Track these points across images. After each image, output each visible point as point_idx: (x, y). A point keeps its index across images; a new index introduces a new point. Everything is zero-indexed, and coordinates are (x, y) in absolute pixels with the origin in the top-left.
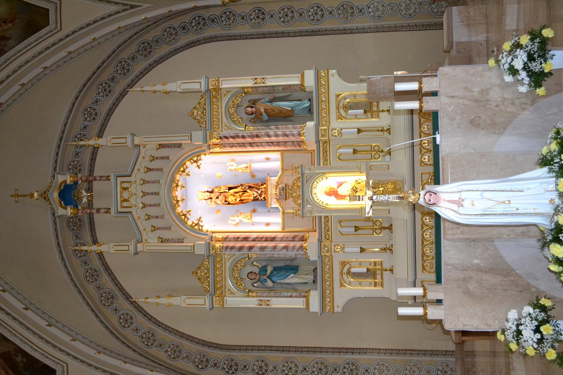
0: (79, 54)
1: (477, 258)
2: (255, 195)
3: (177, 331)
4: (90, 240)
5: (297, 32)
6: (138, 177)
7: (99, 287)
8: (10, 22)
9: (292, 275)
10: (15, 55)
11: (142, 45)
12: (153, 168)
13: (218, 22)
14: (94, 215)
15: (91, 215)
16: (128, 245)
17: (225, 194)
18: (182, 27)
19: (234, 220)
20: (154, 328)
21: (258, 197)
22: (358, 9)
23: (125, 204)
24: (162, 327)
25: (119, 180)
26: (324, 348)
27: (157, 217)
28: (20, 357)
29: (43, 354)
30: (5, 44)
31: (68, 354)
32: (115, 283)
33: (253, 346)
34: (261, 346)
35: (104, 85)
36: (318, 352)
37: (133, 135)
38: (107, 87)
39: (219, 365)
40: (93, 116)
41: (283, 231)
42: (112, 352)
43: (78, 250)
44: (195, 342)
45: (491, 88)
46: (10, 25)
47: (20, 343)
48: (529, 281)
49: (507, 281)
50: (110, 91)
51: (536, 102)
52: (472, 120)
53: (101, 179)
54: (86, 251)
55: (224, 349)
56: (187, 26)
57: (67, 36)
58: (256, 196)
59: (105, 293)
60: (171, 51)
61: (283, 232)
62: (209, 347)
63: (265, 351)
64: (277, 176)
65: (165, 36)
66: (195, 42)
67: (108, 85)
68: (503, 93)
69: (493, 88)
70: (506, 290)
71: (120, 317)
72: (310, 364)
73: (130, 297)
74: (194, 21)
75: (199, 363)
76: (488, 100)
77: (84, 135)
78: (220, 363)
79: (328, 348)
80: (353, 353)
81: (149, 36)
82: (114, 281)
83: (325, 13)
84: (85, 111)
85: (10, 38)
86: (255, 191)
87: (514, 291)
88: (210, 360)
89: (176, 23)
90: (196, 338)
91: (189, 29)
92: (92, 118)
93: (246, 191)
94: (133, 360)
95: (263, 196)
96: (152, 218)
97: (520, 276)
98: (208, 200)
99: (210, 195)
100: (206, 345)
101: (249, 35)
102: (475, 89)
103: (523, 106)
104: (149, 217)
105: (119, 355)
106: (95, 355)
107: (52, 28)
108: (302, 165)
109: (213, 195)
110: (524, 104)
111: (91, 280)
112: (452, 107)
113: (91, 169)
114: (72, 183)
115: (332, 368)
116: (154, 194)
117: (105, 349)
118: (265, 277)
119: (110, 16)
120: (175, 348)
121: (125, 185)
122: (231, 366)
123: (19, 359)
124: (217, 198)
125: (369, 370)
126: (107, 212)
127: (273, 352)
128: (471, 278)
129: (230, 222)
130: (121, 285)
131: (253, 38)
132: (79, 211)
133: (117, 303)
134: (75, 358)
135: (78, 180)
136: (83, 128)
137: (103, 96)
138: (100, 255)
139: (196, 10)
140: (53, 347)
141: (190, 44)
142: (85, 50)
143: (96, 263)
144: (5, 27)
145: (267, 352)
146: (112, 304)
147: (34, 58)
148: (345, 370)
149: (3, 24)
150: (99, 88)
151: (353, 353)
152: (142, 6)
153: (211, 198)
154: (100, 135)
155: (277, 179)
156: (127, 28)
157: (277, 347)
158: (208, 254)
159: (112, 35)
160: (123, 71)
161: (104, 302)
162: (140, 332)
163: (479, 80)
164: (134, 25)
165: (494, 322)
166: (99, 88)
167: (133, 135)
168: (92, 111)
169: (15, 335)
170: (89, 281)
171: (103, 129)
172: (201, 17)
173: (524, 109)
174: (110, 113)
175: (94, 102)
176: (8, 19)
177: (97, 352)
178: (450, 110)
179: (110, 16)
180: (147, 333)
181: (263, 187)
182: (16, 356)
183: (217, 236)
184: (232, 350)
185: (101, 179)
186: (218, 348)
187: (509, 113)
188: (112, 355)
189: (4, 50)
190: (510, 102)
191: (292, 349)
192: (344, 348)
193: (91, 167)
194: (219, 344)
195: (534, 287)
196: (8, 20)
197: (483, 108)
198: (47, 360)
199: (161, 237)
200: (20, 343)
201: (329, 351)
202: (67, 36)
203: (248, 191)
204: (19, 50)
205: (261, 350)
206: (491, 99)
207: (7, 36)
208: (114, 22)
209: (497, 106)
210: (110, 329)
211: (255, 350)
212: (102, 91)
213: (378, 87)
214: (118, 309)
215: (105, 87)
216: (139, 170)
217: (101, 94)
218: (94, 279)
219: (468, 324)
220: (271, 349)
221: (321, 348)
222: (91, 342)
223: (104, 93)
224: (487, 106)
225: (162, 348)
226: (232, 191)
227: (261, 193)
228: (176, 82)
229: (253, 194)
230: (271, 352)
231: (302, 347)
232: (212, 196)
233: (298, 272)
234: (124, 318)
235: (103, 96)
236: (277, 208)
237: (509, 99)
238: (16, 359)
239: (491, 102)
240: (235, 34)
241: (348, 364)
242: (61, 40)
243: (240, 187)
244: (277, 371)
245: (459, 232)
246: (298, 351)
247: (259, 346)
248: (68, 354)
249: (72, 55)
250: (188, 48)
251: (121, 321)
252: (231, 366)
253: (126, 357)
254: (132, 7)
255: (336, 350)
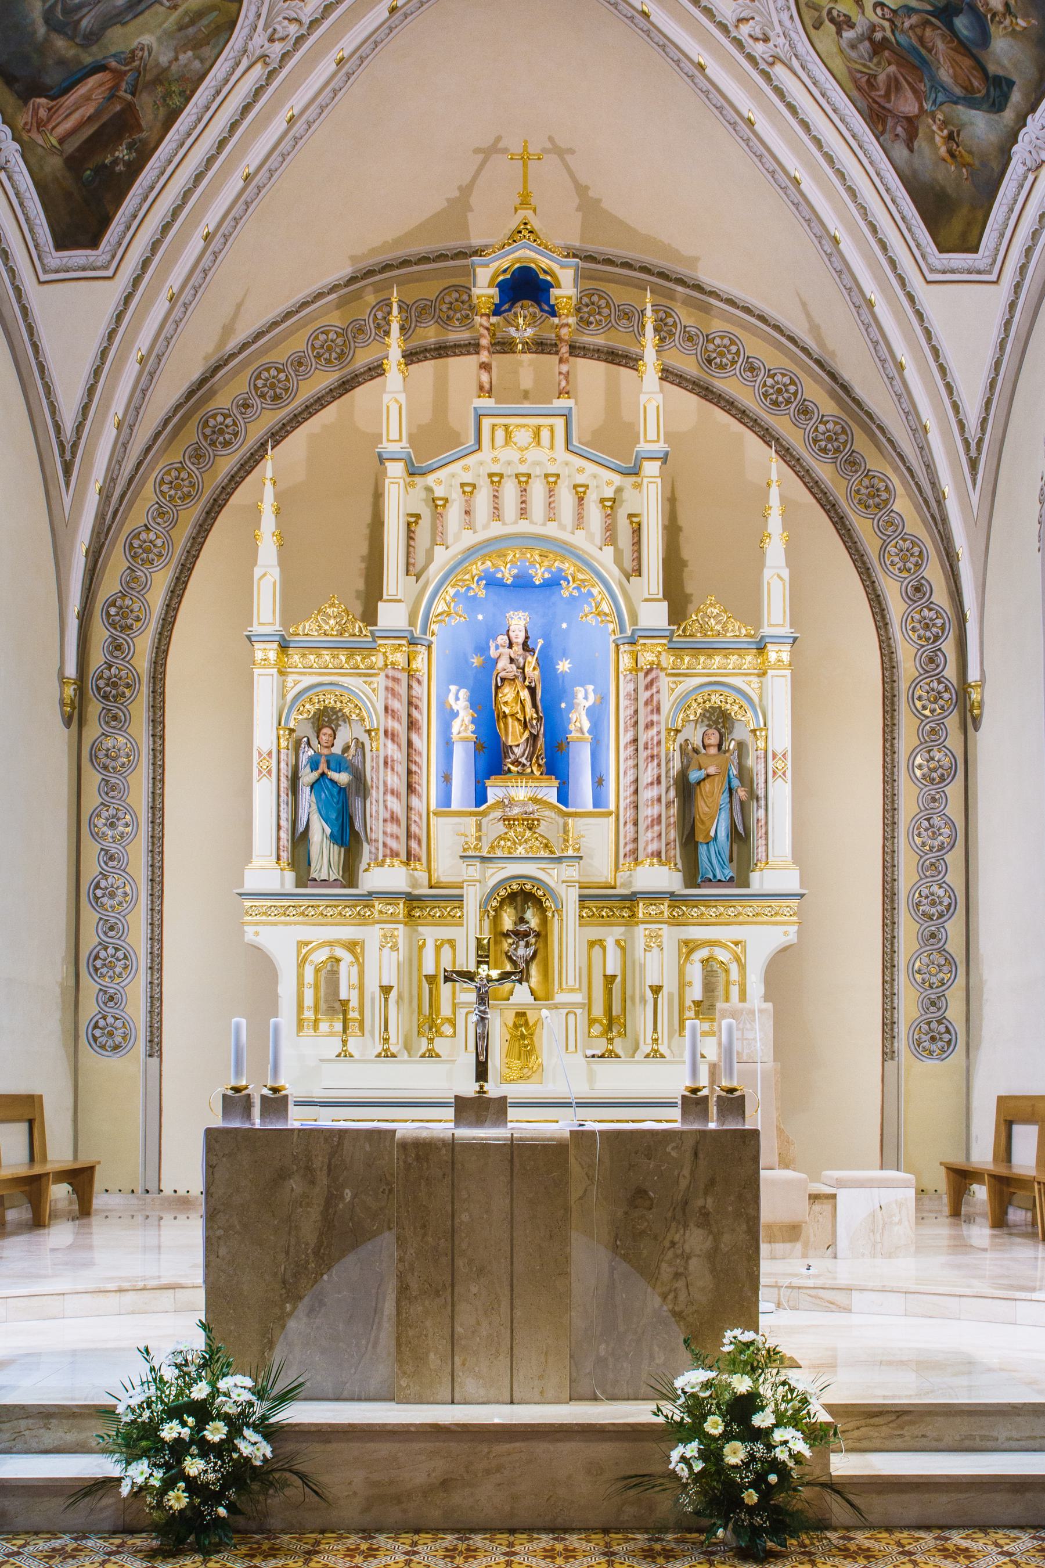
0: (867, 327)
1: (355, 1196)
2: (516, 750)
3: (197, 557)
4: (415, 343)
5: (893, 858)
6: (564, 472)
7: (300, 364)
8: (951, 154)
9: (328, 831)
10: (871, 163)
11: (882, 485)
12: (585, 506)
13: (927, 672)
14: (475, 356)
15: (472, 347)
16: (400, 440)
17: (521, 679)
18: (922, 585)
19: (457, 699)
20: (204, 499)
21: (512, 757)
22: (939, 997)
23: (500, 434)
24: (205, 520)
25: (559, 423)
26: (162, 903)
27: (467, 512)
28: (126, 158)
29: (135, 216)
30: (897, 135)
31: (136, 281)
32: (312, 405)
33: (162, 737)
34: (161, 1005)
35: (792, 388)
36: (152, 889)
37: (665, 459)
38: (785, 395)
39: (116, 657)
40: (718, 360)
41: (431, 814)
42: (144, 392)
43: (389, 313)
44: (171, 599)
45: (711, 1232)
46: (943, 151)
47: (162, 157)
48: (306, 1300)
49: (307, 1255)
50: (775, 403)
51: (677, 1322)
52: (646, 1192)
53: (562, 377)
54: (387, 333)
55: (155, 668)
56: (921, 598)
57: (911, 298)
58: (513, 753)
59: (287, 379)
60: (865, 558)
61: (428, 814)
62: (160, 634)
63: (151, 767)
64: (558, 801)
65: (901, 542)
66: (883, 617)
67: (790, 398)
68: (699, 1256)
69: (711, 1237)
70: (287, 1253)
71: (230, 416)
72: (124, 871)
73: (278, 443)
74: (932, 614)
75: (122, 608)
76: (686, 1226)
77: (671, 334)
78: (123, 659)
79: (161, 911)
80: (150, 968)
81: (902, 505)
82: (316, 402)
83: (932, 923)
84: (730, 339)
85: (911, 150)
86: (525, 750)
87: (285, 1268)
88: (128, 635)
89: (934, 573)
90: (180, 602)
91: (916, 602)
92: (714, 355)
93: (525, 727)
94: (125, 445)
95: (512, 768)
96: (466, 501)
97: (316, 1281)
98: (506, 637)
99: (517, 643)
100: (163, 626)
101: (892, 745)
102: (710, 1201)
103: (671, 1296)
104: (469, 489)
105: (138, 409)
106: (135, 349)
107: (931, 260)
108: (581, 858)
109: (518, 649)
110: (676, 1297)
111: (318, 343)
112: (674, 1154)
113: (589, 350)
114: (552, 302)
115: (115, 920)
116: (524, 506)
117: (152, 375)
118: (323, 767)
119: (956, 407)
120: (155, 550)
121: (545, 434)
122: (115, 685)
123: (122, 153)
124: (512, 660)
125: (111, 1004)
126: (481, 388)
127: (151, 785)
128: (313, 1183)
129: (453, 688)
130: (306, 419)
131: (885, 754)
132: (485, 318)
133: (263, 408)
134: (128, 299)
135: (560, 316)
136: (689, 332)
137: (765, 385)
138: (376, 371)
139: (958, 619)
140: (153, 243)
141: (880, 603)
142: (875, 343)
143: (362, 359)
144: (938, 139)
145: (151, 771)
146: (259, 396)
147: (862, 211)
148: (111, 951)
149: (946, 132)
150: (784, 375)
151: (150, 968)
152: (974, 489)
153: (511, 646)
154: (668, 375)
155: (549, 800)
156: (924, 449)
157: (162, 795)
158: (378, 634)
159: (911, 412)
160: (822, 437)
161: (265, 375)
162: (193, 464)
163: (730, 1209)
164: (930, 467)
165: (219, 1228)
166: (784, 375)
167: (665, 459)
168: (729, 357)
169: (182, 145)
170: (316, 338)
171: (685, 384)
172: (943, 633)
173: (664, 1297)
174: (723, 404)
175: (751, 363)
176: (958, 146)
177: (143, 356)
178: (669, 1149)
179: (956, 407)
180: (191, 482)
181: (535, 768)
182: (130, 147)
183: (421, 657)
184: (154, 687)
185: (562, 377)
186: (157, 653)
187: (658, 1267)
188: (130, 411)
189: (882, 133)
190: (681, 1270)
191: (158, 829)
192: (161, 948)
193: (594, 350)
194: (166, 658)
195: (295, 1308)
196: (955, 147)
197: (670, 1214)
198: (122, 227)
199: (420, 521)
200: (162, 157)
201: (155, 915)
202: (911, 298)
203: (526, 735)
204: (882, 173)
205: (155, 756)
206: (688, 1233)
207: (916, 144)
208: (942, 419)
209: (673, 1244)
210: (198, 389)
211: (154, 742)
212: (777, 383)
213: (748, 1026)
214: (249, 411)
215: (787, 391)
216: (581, 470)
217: (770, 382)
218: (322, 351)
219: (216, 1176)
220: (158, 779)
221: (161, 897)
222: (168, 341)
223: (772, 387)
224: (674, 1224)
225: (154, 519)
226: (525, 694)
227: (520, 763)
228: (788, 565)
229: (518, 745)
230: (151, 781)
231: (162, 853)
232: (515, 648)
233: (336, 846)
234: (227, 426)
235: (765, 385)
236: (486, 801)
237: (686, 1269)
238: (121, 145)
239: (682, 1232)
240: (896, 713)
241: (125, 957)
242: (902, 281)
243: (535, 716)
244: (107, 794)
245: (410, 1160)
246: (153, 844)
247: (163, 752)
248: (136, 281)
249: (865, 310)
250: (869, 600)
251: (220, 419)
252: (115, 685)
253: (131, 427)
254: (973, 464)
255: (157, 931)
